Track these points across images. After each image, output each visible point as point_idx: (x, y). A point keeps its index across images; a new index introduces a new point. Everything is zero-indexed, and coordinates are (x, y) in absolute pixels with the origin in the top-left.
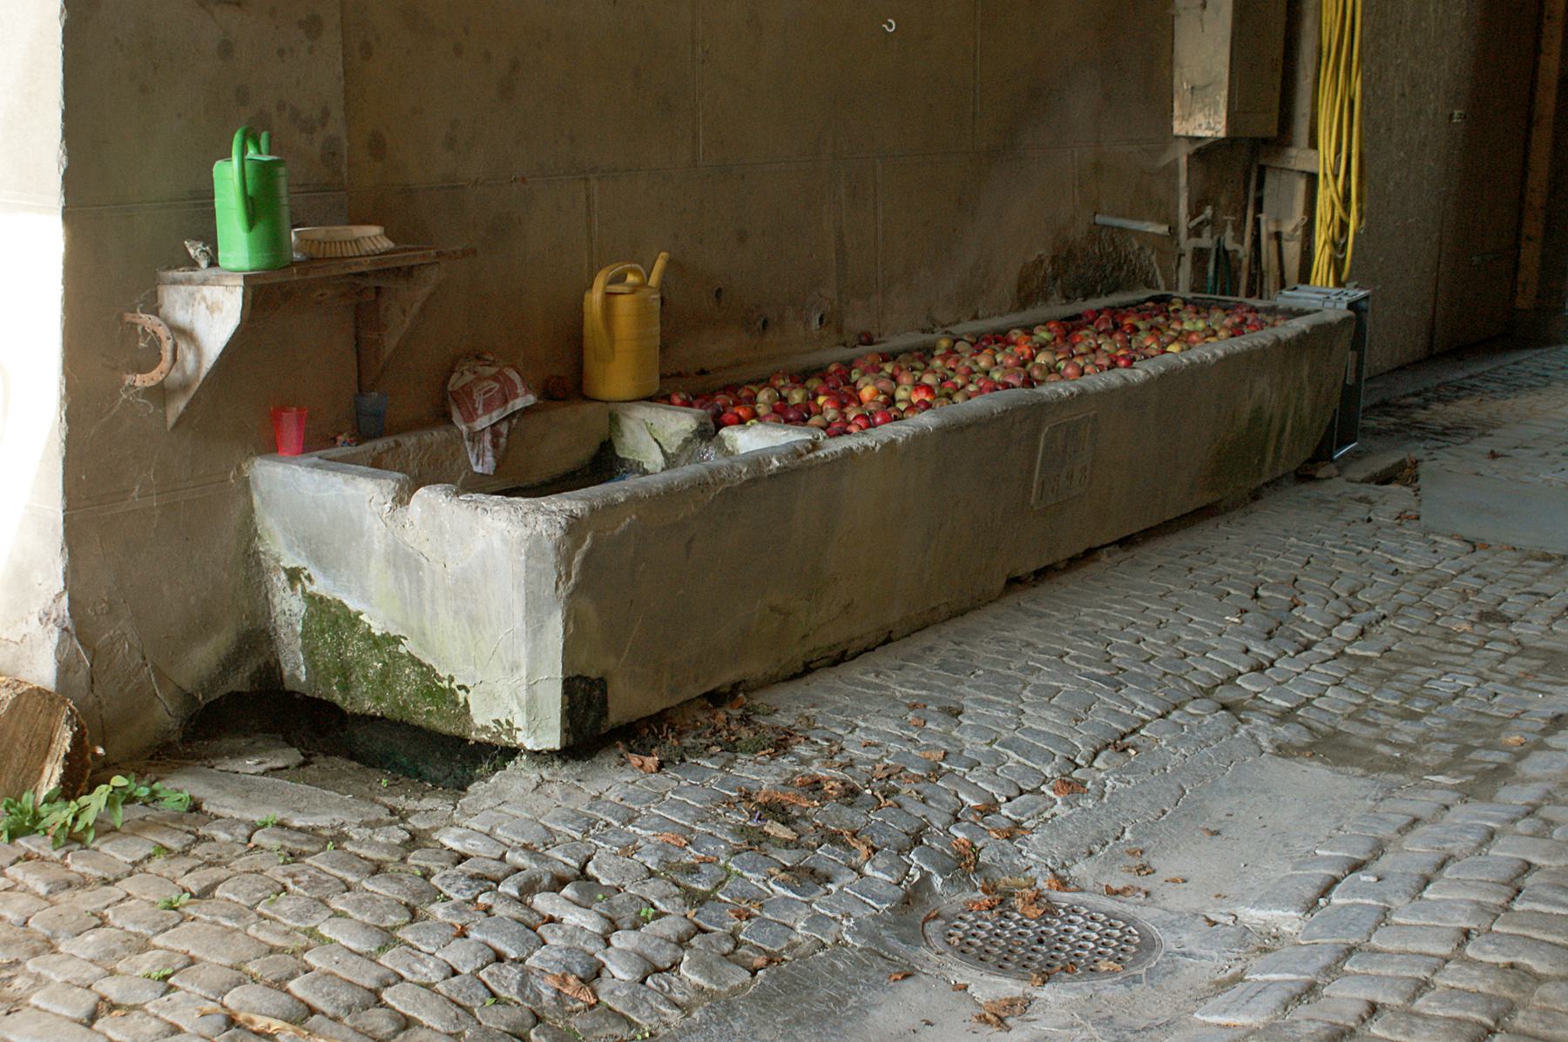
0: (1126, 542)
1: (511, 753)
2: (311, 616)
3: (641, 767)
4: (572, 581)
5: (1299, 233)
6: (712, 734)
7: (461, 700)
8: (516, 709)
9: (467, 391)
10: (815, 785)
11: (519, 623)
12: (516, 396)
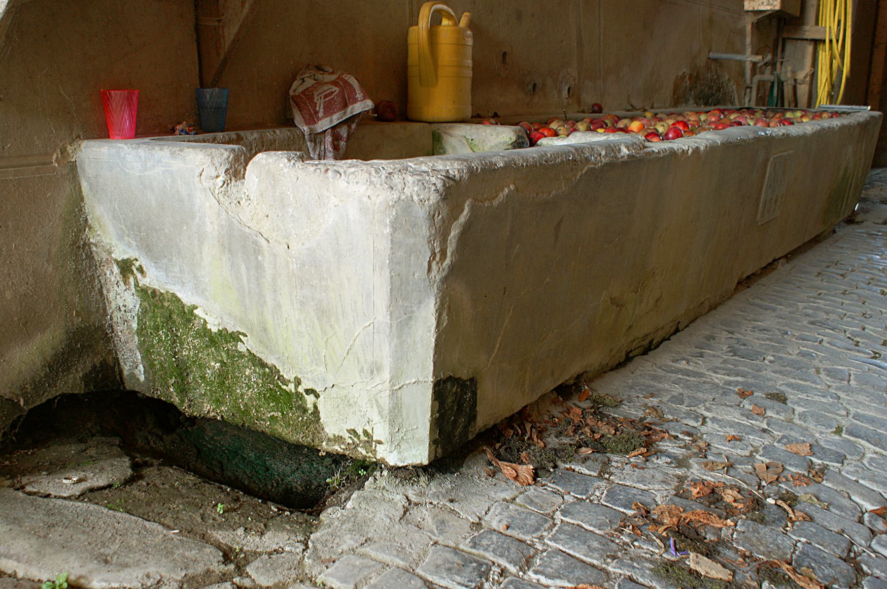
0: (789, 256)
1: (369, 467)
2: (144, 312)
3: (516, 478)
4: (448, 261)
5: (808, 79)
6: (575, 432)
7: (310, 406)
8: (376, 418)
9: (308, 95)
10: (713, 496)
11: (381, 314)
12: (355, 101)
